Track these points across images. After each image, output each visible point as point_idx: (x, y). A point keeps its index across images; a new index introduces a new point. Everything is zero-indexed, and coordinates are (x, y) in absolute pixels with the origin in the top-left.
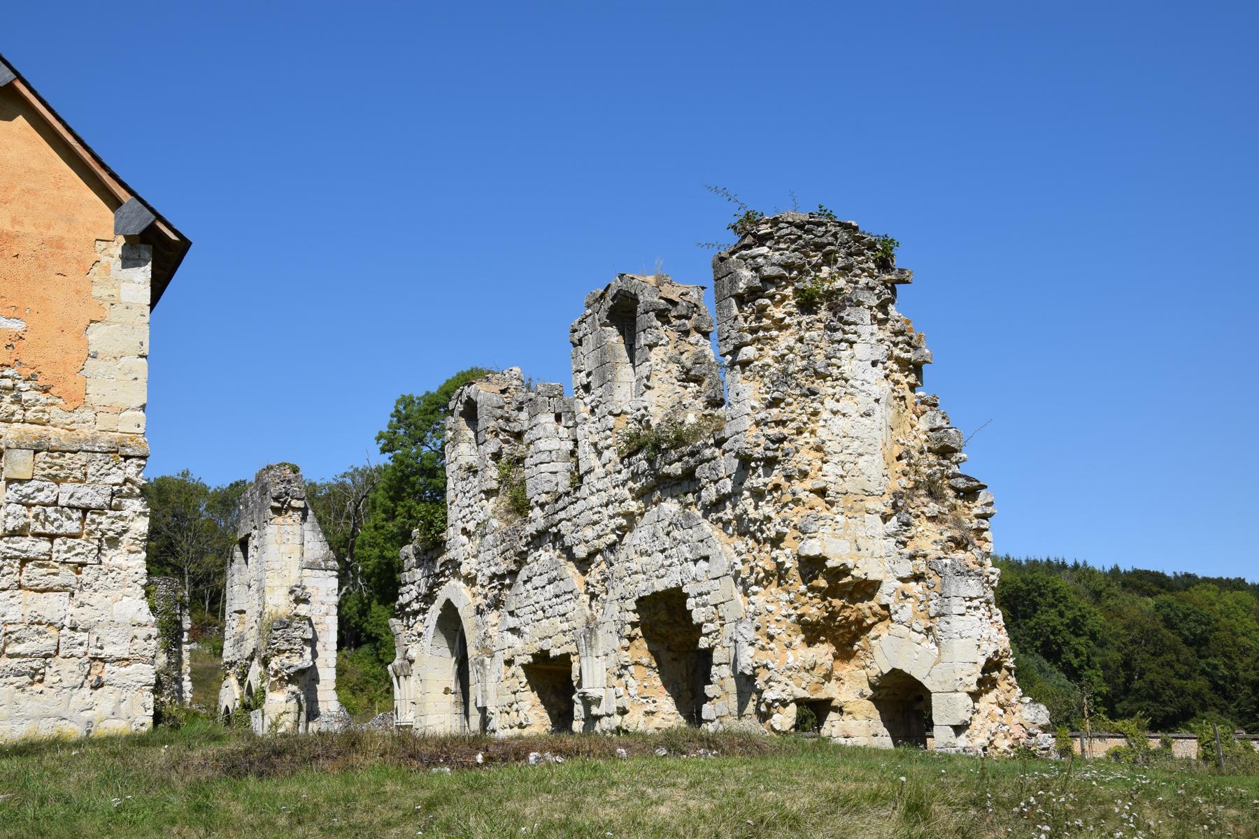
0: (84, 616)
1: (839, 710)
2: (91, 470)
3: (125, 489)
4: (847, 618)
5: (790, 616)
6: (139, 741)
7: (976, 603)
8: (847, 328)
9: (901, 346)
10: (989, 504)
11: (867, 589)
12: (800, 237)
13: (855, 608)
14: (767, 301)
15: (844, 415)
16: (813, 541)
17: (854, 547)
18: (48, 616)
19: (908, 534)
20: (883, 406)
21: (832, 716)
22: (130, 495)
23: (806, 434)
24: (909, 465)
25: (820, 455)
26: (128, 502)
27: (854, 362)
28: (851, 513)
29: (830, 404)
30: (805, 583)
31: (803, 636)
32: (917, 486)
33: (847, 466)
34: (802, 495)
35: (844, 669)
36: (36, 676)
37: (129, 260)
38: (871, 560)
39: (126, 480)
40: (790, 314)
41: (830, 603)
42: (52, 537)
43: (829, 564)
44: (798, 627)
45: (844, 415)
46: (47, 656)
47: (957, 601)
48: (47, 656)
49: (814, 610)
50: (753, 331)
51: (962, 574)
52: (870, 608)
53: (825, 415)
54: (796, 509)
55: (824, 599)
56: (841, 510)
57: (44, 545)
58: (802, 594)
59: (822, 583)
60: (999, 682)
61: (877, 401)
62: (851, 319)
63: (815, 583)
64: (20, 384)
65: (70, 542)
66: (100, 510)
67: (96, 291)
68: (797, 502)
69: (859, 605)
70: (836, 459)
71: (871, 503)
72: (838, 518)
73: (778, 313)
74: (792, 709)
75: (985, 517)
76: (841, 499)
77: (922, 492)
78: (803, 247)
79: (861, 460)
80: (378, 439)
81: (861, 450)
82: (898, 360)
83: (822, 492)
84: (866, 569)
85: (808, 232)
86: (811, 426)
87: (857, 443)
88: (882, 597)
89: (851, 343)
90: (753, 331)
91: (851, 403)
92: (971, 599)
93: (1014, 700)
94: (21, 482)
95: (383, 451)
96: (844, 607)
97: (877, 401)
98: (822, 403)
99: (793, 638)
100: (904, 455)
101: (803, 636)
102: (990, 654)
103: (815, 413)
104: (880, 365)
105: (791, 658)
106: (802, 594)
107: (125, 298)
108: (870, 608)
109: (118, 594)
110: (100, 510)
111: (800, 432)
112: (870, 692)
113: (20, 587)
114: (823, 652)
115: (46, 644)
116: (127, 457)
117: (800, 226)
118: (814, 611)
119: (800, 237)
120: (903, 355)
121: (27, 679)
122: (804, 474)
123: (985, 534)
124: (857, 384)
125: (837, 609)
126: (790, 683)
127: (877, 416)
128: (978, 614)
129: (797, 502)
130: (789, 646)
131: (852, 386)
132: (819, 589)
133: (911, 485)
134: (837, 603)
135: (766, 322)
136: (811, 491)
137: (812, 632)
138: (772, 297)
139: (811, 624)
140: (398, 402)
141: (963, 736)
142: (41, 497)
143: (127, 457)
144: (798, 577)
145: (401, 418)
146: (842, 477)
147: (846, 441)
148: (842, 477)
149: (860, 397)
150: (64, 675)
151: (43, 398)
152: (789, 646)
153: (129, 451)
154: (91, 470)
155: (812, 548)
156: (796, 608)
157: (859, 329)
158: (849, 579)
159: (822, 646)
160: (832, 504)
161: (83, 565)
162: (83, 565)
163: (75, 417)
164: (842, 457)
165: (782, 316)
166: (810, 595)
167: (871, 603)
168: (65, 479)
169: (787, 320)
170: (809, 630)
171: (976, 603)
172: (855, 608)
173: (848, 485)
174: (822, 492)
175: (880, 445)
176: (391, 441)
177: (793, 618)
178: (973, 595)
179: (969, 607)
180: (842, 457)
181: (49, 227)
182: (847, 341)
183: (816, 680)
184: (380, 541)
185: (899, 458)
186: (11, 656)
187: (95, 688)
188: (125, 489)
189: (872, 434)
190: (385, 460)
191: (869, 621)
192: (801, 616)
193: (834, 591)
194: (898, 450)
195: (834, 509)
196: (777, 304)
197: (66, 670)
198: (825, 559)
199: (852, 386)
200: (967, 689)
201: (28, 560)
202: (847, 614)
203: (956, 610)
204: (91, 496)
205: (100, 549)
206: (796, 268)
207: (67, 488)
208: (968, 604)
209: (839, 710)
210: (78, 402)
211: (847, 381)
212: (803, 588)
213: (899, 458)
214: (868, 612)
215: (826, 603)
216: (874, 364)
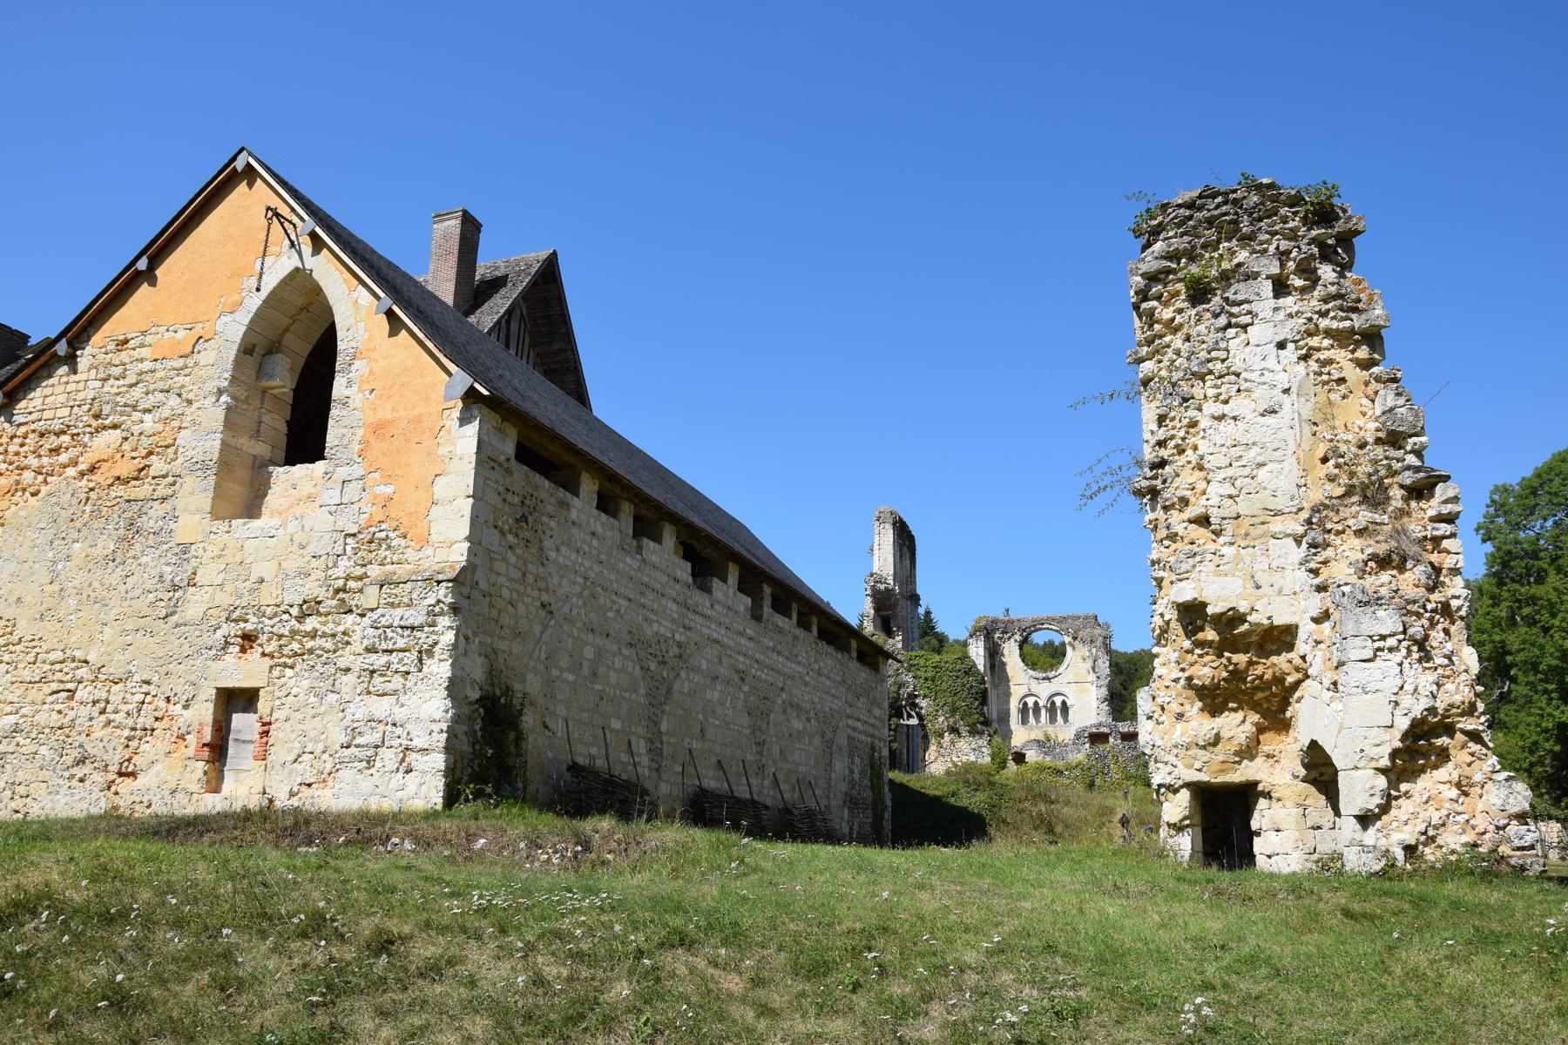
0: (399, 714)
1: (1268, 795)
2: (414, 596)
3: (437, 609)
4: (1261, 677)
5: (1176, 680)
6: (430, 816)
7: (1392, 642)
8: (1235, 310)
9: (1332, 314)
10: (1455, 499)
11: (1280, 638)
12: (1190, 218)
13: (1268, 663)
14: (1154, 303)
15: (1235, 418)
16: (1184, 583)
17: (1250, 585)
18: (379, 715)
19: (1319, 559)
20: (1294, 396)
21: (1262, 803)
22: (442, 613)
23: (1189, 452)
24: (1337, 466)
25: (1203, 474)
26: (440, 619)
27: (1248, 349)
28: (1246, 541)
29: (1211, 408)
30: (1188, 637)
31: (1199, 704)
32: (1349, 492)
33: (1238, 483)
34: (1179, 529)
35: (1270, 742)
36: (370, 762)
37: (464, 420)
38: (1279, 599)
39: (439, 601)
40: (1180, 311)
41: (1229, 659)
42: (391, 651)
43: (1210, 610)
44: (1191, 693)
45: (1235, 418)
46: (377, 747)
47: (1358, 642)
48: (377, 747)
49: (1206, 670)
50: (1149, 342)
51: (1367, 604)
52: (1290, 662)
53: (1204, 422)
54: (1174, 546)
55: (1220, 656)
56: (1228, 539)
57: (384, 659)
58: (1187, 652)
59: (1210, 634)
60: (1452, 751)
61: (1286, 391)
62: (1239, 297)
63: (1200, 636)
64: (392, 535)
65: (401, 655)
66: (420, 628)
67: (442, 451)
68: (1173, 537)
69: (1274, 659)
70: (1221, 475)
71: (1277, 525)
72: (1226, 550)
73: (1167, 314)
74: (1185, 795)
75: (1450, 519)
76: (1229, 527)
77: (1355, 499)
78: (1194, 227)
79: (1262, 474)
80: (1477, 530)
81: (1260, 459)
82: (1328, 333)
83: (1203, 521)
84: (1269, 610)
85: (1200, 209)
86: (1191, 440)
87: (1255, 450)
88: (1302, 647)
89: (1245, 327)
90: (1149, 342)
91: (1247, 401)
92: (1383, 638)
93: (1478, 778)
94: (372, 610)
95: (1484, 541)
96: (1250, 663)
97: (1286, 391)
98: (1200, 410)
99: (1187, 707)
100: (1330, 454)
101: (1199, 704)
102: (1417, 712)
103: (1193, 424)
104: (1291, 346)
105: (1181, 733)
106: (1187, 652)
107: (459, 452)
108: (1290, 662)
109: (428, 695)
110: (420, 628)
111: (1181, 451)
112: (1303, 772)
113: (369, 693)
114: (1236, 725)
115: (375, 737)
116: (439, 582)
117: (1190, 205)
118: (1207, 670)
119: (1190, 218)
120: (1335, 325)
121: (364, 764)
122: (1185, 502)
123: (1445, 543)
124: (1254, 376)
125: (1242, 666)
126: (1179, 764)
127: (1287, 412)
128: (1398, 657)
129: (1173, 537)
130: (1180, 716)
131: (1246, 380)
132: (1209, 644)
133: (1340, 491)
134: (1241, 659)
135: (1157, 327)
136: (1190, 521)
137: (1214, 699)
138: (1159, 298)
139: (1203, 687)
140: (1493, 492)
141: (1372, 831)
142: (383, 621)
143: (439, 582)
144: (1180, 631)
145: (1499, 507)
146: (1231, 497)
147: (1235, 452)
148: (1231, 497)
149: (1259, 392)
150: (387, 762)
151: (403, 542)
152: (1180, 716)
153: (440, 577)
154: (414, 596)
155: (1185, 592)
156: (1183, 670)
157: (1255, 307)
158: (1246, 626)
159: (1233, 715)
160: (1217, 533)
161: (408, 673)
162: (408, 673)
163: (421, 554)
164: (1230, 472)
165: (1170, 315)
166: (1198, 651)
167: (1290, 656)
168: (399, 605)
169: (1178, 319)
170: (1208, 696)
171: (1392, 642)
172: (1268, 663)
173: (1242, 507)
174: (1203, 521)
175: (1292, 447)
176: (1488, 531)
177: (1182, 682)
178: (1385, 632)
179: (1379, 649)
180: (1230, 472)
181: (414, 408)
182: (1237, 326)
183: (1221, 758)
184: (1488, 626)
185: (1325, 460)
186: (357, 746)
187: (407, 772)
188: (437, 609)
189: (1280, 435)
190: (1489, 547)
191: (1290, 679)
192: (1190, 679)
193: (1229, 643)
194: (1321, 450)
195: (1221, 540)
196: (1166, 304)
197: (388, 757)
198: (1204, 605)
199: (1246, 380)
200: (1374, 764)
201: (373, 672)
202: (1259, 672)
203: (1355, 654)
204: (416, 617)
205: (420, 660)
206: (1183, 255)
207: (399, 612)
208: (1377, 644)
209: (1268, 795)
210: (425, 541)
211: (1238, 375)
212: (1187, 644)
213: (1325, 460)
214: (1286, 667)
215: (1224, 660)
216: (1281, 345)
